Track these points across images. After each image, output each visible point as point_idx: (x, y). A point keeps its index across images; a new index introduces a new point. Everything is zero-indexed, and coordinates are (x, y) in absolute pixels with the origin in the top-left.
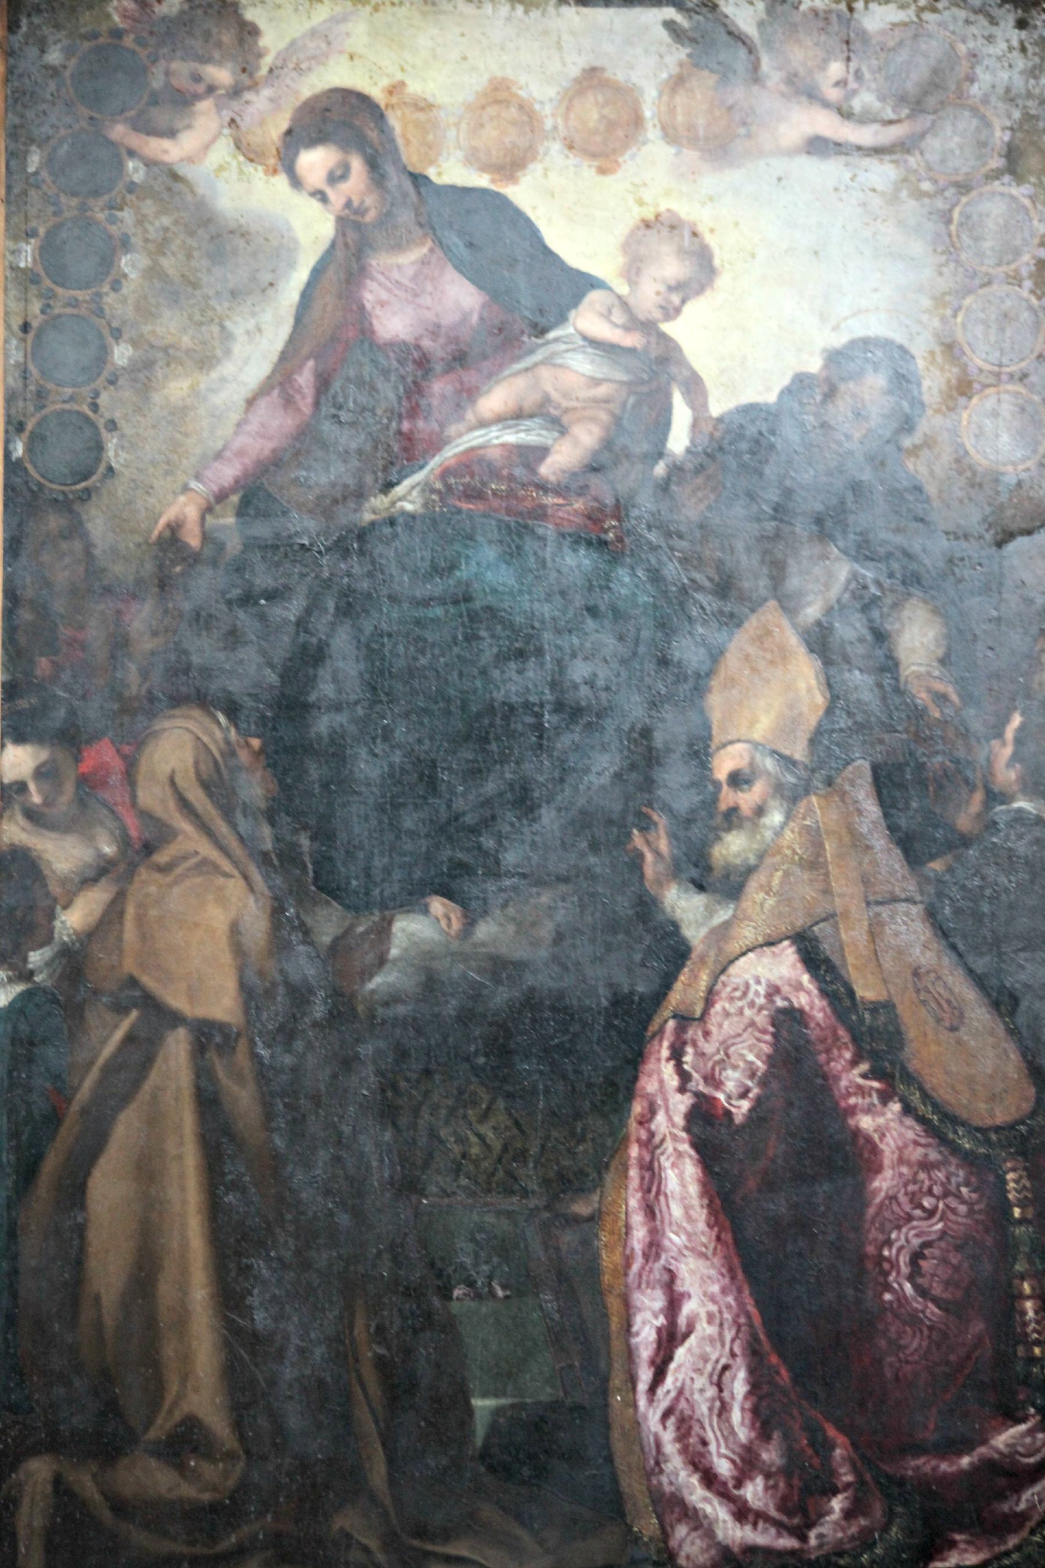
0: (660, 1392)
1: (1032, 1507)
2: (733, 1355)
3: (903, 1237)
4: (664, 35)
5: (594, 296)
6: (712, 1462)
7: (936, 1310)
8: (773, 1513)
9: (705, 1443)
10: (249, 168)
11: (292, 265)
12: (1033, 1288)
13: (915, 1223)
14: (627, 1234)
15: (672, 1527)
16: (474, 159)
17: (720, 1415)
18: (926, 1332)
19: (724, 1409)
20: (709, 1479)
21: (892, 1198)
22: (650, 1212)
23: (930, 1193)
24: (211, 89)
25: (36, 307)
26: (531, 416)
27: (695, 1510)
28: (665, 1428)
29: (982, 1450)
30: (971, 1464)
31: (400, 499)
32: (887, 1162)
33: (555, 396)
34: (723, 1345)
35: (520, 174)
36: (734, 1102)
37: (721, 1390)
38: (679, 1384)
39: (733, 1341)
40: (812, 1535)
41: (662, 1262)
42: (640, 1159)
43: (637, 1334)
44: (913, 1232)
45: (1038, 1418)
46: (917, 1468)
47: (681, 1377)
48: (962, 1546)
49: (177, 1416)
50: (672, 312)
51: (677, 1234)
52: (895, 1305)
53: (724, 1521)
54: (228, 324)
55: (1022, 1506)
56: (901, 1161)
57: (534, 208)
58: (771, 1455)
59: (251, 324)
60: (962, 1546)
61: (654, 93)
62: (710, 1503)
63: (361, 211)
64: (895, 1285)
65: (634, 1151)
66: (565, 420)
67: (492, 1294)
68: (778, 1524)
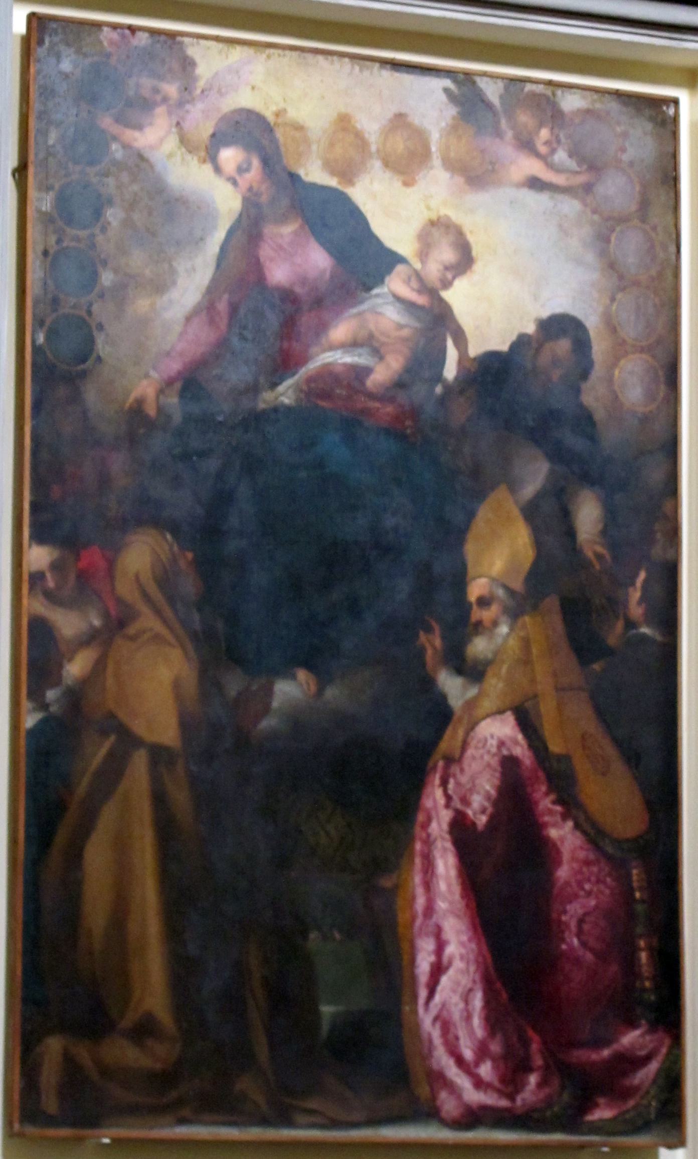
0: (432, 1005)
4: (443, 98)
5: (400, 268)
10: (189, 157)
16: (330, 167)
19: (468, 1018)
20: (460, 1061)
21: (567, 883)
25: (53, 239)
26: (361, 345)
33: (377, 334)
57: (365, 204)
58: (496, 1047)
63: (258, 194)
66: (382, 350)
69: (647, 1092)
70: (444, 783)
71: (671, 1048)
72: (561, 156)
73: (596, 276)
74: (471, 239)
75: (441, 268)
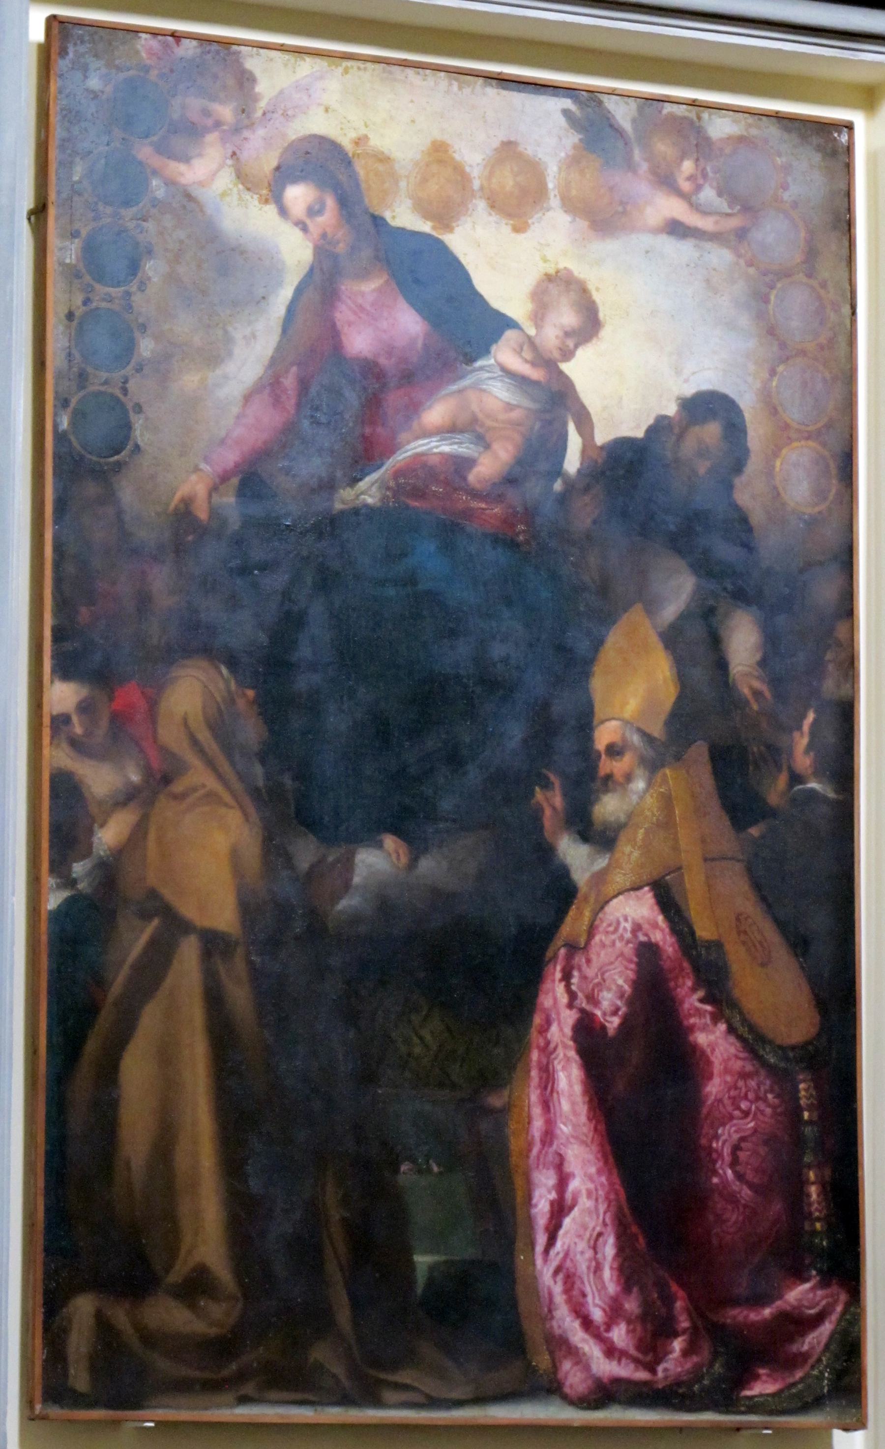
0: (552, 1253)
1: (812, 1348)
2: (605, 1224)
3: (726, 1132)
4: (562, 121)
5: (510, 335)
6: (589, 1311)
7: (749, 1192)
8: (632, 1351)
9: (584, 1295)
10: (247, 196)
11: (280, 284)
12: (816, 1176)
13: (735, 1122)
14: (529, 1123)
15: (561, 1362)
16: (424, 209)
17: (595, 1272)
18: (741, 1209)
19: (598, 1269)
20: (587, 1323)
21: (719, 1101)
22: (546, 1105)
23: (746, 1097)
24: (218, 124)
25: (79, 299)
26: (462, 431)
27: (577, 1348)
28: (555, 1282)
29: (779, 1303)
30: (771, 1314)
31: (362, 493)
32: (716, 1071)
33: (480, 416)
34: (598, 1218)
35: (454, 224)
36: (608, 1018)
37: (596, 1253)
38: (566, 1247)
39: (605, 1213)
40: (660, 1369)
41: (555, 1147)
42: (539, 1062)
43: (536, 1206)
44: (733, 1129)
45: (818, 1278)
46: (734, 1318)
47: (567, 1241)
48: (764, 1378)
49: (191, 1264)
50: (568, 355)
51: (565, 1124)
52: (721, 1187)
53: (598, 1358)
54: (230, 329)
55: (806, 1347)
56: (726, 1071)
58: (631, 1305)
59: (248, 331)
60: (764, 1378)
61: (555, 169)
62: (588, 1344)
64: (721, 1171)
65: (535, 1055)
67: (429, 1170)
68: (636, 1361)
69: (819, 1360)
70: (567, 977)
71: (847, 1306)
72: (708, 194)
73: (751, 344)
74: (596, 297)
75: (561, 334)
